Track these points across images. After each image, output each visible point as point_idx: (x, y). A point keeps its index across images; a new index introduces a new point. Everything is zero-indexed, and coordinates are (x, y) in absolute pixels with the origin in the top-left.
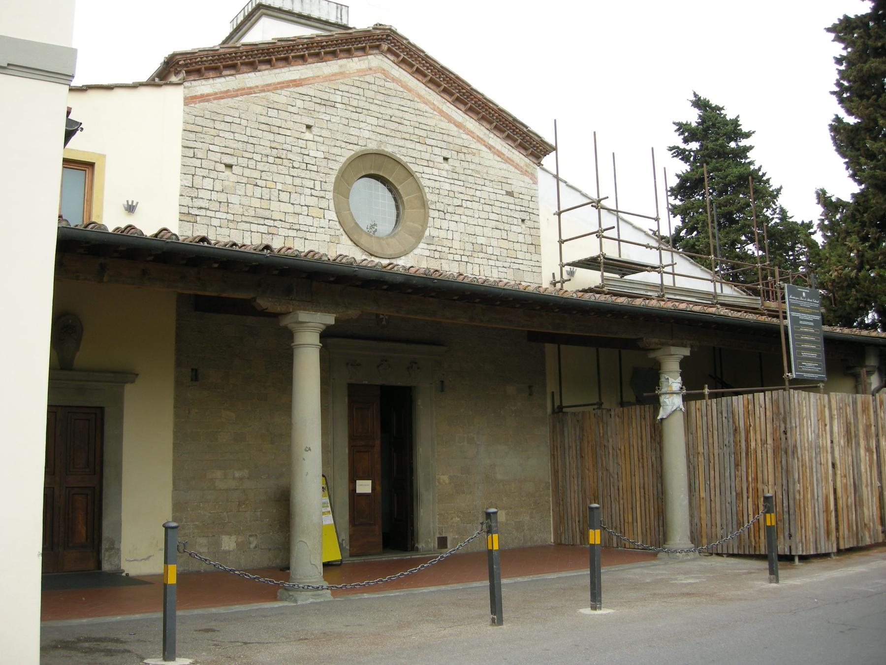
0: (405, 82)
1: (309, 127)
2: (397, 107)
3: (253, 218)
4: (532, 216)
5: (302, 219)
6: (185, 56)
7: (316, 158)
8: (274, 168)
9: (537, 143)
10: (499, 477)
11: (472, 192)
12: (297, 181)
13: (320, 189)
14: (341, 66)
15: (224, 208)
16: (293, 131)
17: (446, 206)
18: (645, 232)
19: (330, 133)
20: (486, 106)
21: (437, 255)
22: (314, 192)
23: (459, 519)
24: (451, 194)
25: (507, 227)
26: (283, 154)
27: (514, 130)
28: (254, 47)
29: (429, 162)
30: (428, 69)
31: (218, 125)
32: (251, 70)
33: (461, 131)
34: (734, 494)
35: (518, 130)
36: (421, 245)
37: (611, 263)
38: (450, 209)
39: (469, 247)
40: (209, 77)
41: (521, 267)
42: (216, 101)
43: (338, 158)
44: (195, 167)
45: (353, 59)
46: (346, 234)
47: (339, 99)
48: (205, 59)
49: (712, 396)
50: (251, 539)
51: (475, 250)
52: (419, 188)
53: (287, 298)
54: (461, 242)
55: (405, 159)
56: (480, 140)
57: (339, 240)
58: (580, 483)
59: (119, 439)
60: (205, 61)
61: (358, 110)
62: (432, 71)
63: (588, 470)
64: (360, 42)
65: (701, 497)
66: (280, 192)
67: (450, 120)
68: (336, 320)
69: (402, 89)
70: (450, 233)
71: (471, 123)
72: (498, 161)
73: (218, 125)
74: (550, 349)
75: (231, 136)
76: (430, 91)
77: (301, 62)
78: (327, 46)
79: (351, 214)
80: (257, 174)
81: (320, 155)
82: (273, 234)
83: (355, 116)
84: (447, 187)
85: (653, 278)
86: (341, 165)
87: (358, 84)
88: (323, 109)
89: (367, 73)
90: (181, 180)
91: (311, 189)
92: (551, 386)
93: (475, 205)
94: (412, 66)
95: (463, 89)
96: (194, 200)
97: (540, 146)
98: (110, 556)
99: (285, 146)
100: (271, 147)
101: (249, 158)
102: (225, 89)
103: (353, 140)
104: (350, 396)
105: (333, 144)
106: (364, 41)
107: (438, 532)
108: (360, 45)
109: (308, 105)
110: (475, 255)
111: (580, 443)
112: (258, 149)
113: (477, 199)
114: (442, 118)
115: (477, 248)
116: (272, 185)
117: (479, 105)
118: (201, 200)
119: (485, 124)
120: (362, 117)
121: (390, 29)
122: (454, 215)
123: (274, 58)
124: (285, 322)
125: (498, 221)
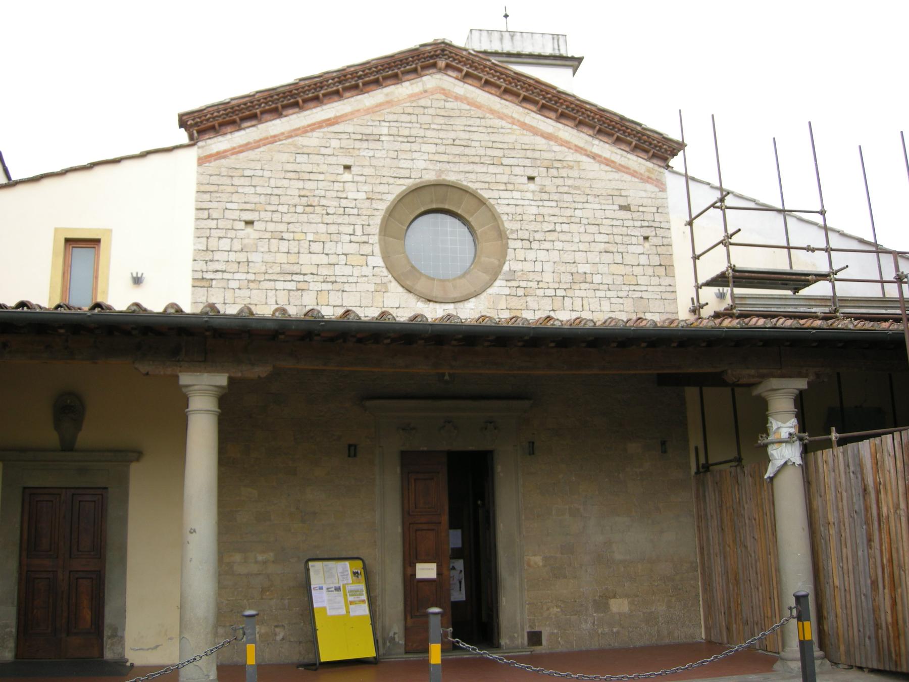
0: (473, 98)
1: (347, 167)
2: (462, 128)
3: (278, 275)
4: (659, 231)
5: (338, 270)
6: (192, 115)
7: (356, 200)
8: (304, 218)
9: (659, 142)
10: (618, 557)
11: (569, 212)
12: (333, 229)
13: (362, 233)
14: (387, 95)
15: (243, 268)
16: (327, 175)
17: (532, 233)
18: (839, 232)
19: (373, 170)
20: (582, 108)
21: (520, 292)
22: (353, 238)
23: (559, 610)
24: (540, 218)
25: (622, 248)
26: (315, 201)
27: (624, 132)
28: (272, 92)
29: (508, 186)
30: (499, 78)
31: (236, 181)
32: (275, 117)
33: (552, 143)
34: (869, 582)
35: (629, 131)
36: (498, 283)
37: (748, 276)
38: (538, 236)
39: (569, 278)
40: (226, 132)
41: (645, 295)
42: (234, 157)
43: (384, 197)
44: (210, 229)
45: (403, 84)
46: (396, 280)
47: (385, 131)
48: (216, 114)
49: (842, 442)
50: (277, 630)
51: (575, 281)
52: (495, 217)
53: (174, 359)
54: (555, 274)
55: (472, 186)
56: (578, 149)
57: (386, 287)
58: (722, 563)
59: (123, 521)
60: (217, 116)
61: (410, 139)
62: (505, 80)
63: (729, 546)
64: (408, 64)
65: (835, 585)
66: (311, 243)
67: (535, 131)
68: (809, 383)
69: (468, 107)
70: (539, 264)
71: (566, 132)
72: (606, 172)
73: (236, 181)
74: (691, 393)
75: (252, 190)
76: (507, 103)
77: (336, 98)
78: (366, 75)
79: (407, 258)
80: (283, 227)
81: (362, 196)
82: (302, 290)
83: (407, 146)
84: (534, 210)
85: (821, 289)
86: (388, 204)
87: (410, 110)
88: (365, 145)
89: (421, 96)
90: (194, 244)
91: (350, 235)
92: (695, 440)
93: (574, 228)
94: (480, 79)
95: (547, 93)
96: (209, 263)
97: (664, 145)
98: (113, 644)
99: (317, 193)
100: (300, 196)
101: (273, 211)
102: (245, 142)
103: (406, 173)
104: (403, 466)
105: (378, 181)
106: (413, 62)
107: (528, 626)
108: (408, 67)
109: (344, 143)
110: (576, 286)
111: (720, 512)
112: (283, 199)
113: (577, 220)
114: (525, 132)
115: (578, 278)
116: (302, 237)
117: (573, 109)
118: (217, 263)
119: (585, 129)
120: (415, 147)
121: (443, 43)
122: (544, 242)
123: (300, 100)
124: (759, 390)
125: (608, 243)
